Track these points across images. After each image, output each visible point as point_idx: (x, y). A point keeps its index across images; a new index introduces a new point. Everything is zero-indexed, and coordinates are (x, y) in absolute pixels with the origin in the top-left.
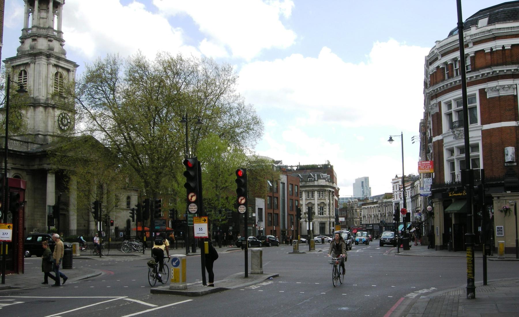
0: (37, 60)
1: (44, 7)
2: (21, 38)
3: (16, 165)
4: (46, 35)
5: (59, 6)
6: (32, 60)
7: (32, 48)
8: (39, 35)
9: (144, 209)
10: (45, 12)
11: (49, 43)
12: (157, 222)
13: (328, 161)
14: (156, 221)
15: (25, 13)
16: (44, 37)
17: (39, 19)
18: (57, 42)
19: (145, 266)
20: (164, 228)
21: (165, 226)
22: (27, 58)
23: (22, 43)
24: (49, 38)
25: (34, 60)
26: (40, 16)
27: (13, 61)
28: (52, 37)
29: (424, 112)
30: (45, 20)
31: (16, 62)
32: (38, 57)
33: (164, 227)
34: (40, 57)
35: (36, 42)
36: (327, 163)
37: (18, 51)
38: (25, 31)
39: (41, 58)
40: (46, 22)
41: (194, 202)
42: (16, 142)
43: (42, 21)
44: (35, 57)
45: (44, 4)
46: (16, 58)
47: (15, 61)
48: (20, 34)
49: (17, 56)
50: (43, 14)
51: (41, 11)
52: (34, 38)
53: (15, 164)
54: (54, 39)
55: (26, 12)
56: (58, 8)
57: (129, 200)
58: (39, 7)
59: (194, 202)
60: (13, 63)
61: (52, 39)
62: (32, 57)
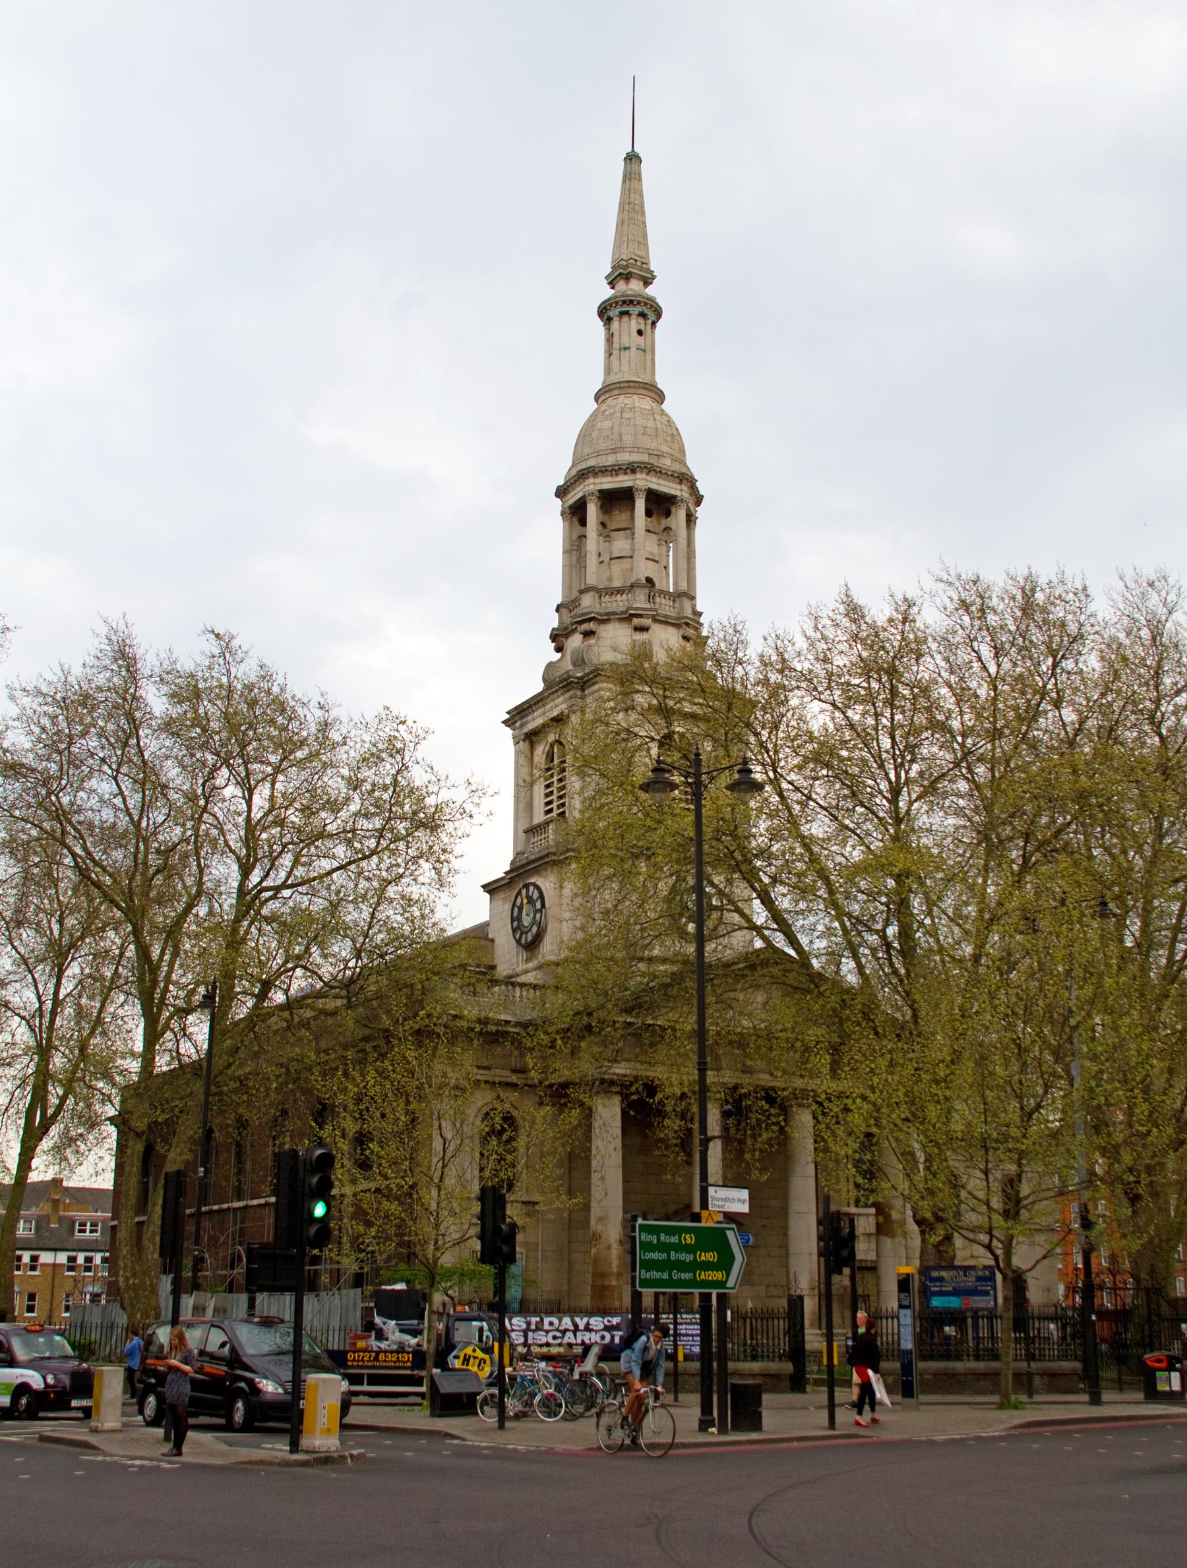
2: (554, 637)
3: (493, 1072)
4: (625, 613)
5: (673, 509)
6: (573, 701)
8: (601, 615)
9: (152, 1399)
10: (626, 538)
11: (639, 637)
15: (564, 552)
16: (621, 620)
17: (609, 564)
20: (980, 1305)
21: (986, 1293)
23: (559, 649)
24: (636, 621)
25: (579, 702)
26: (611, 553)
27: (527, 715)
28: (647, 617)
29: (554, 629)
30: (625, 564)
31: (534, 719)
33: (978, 1302)
34: (596, 687)
35: (592, 641)
38: (564, 611)
42: (525, 993)
43: (617, 567)
44: (583, 690)
46: (524, 710)
47: (530, 717)
48: (554, 621)
50: (620, 545)
51: (614, 534)
52: (585, 627)
53: (488, 1068)
54: (655, 620)
57: (176, 1332)
60: (526, 723)
61: (646, 622)
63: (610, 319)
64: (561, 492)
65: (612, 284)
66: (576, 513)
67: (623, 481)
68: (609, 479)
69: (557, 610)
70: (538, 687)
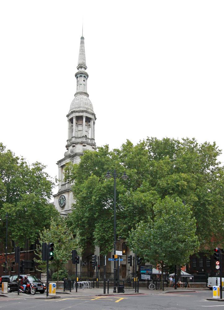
0: (74, 160)
1: (80, 122)
2: (66, 147)
7: (72, 152)
12: (143, 268)
13: (128, 140)
14: (142, 267)
16: (80, 144)
18: (90, 146)
19: (217, 281)
22: (69, 159)
24: (83, 144)
32: (75, 157)
34: (76, 157)
35: (74, 148)
36: (212, 144)
37: (65, 155)
38: (68, 141)
39: (76, 158)
40: (82, 133)
41: (218, 265)
44: (73, 158)
45: (80, 121)
49: (65, 158)
51: (78, 125)
52: (73, 145)
54: (87, 144)
55: (69, 128)
56: (91, 122)
58: (77, 123)
59: (218, 265)
61: (86, 144)
62: (70, 158)
63: (77, 77)
64: (68, 116)
65: (78, 69)
66: (71, 121)
67: (81, 114)
68: (78, 114)
69: (67, 141)
70: (63, 157)
